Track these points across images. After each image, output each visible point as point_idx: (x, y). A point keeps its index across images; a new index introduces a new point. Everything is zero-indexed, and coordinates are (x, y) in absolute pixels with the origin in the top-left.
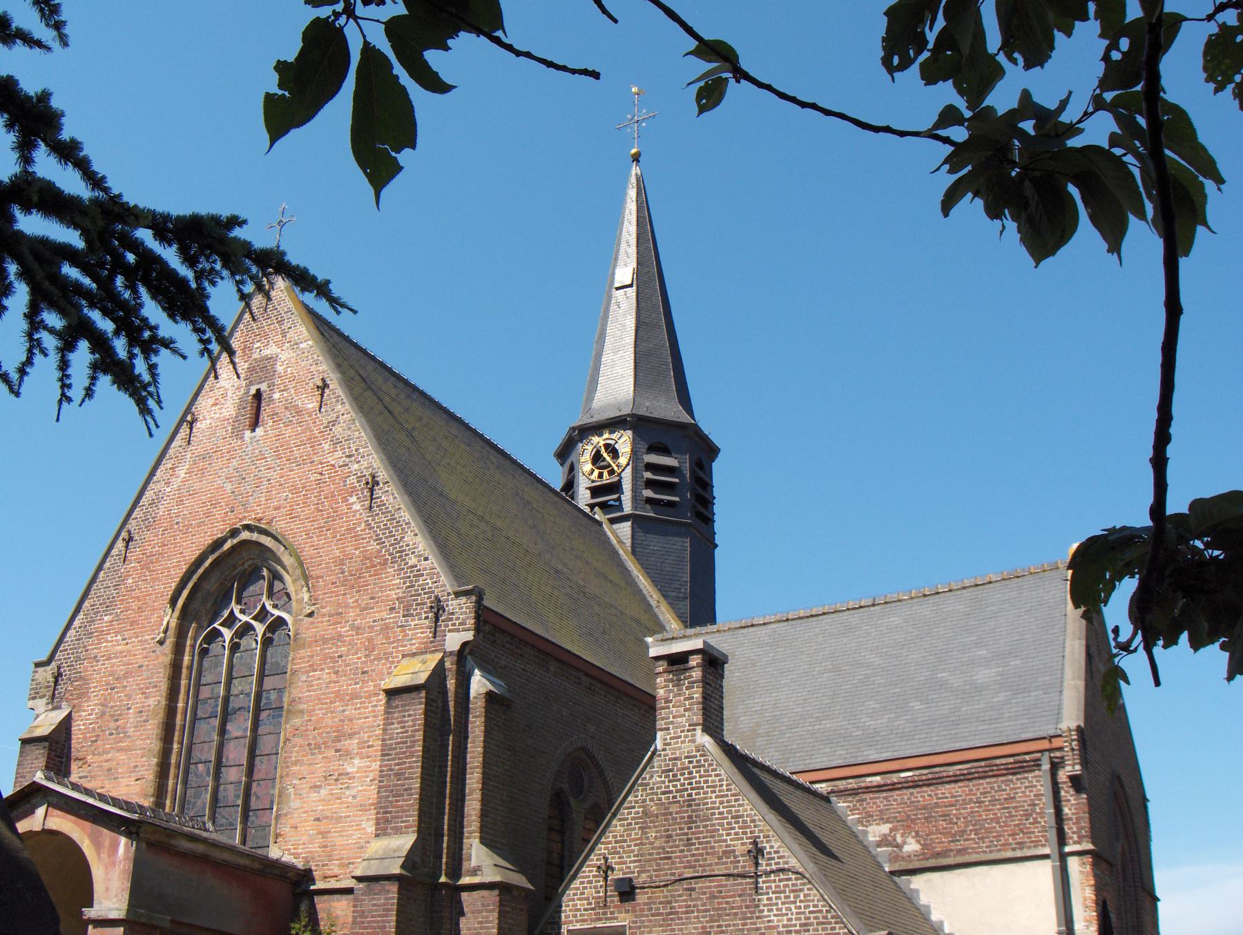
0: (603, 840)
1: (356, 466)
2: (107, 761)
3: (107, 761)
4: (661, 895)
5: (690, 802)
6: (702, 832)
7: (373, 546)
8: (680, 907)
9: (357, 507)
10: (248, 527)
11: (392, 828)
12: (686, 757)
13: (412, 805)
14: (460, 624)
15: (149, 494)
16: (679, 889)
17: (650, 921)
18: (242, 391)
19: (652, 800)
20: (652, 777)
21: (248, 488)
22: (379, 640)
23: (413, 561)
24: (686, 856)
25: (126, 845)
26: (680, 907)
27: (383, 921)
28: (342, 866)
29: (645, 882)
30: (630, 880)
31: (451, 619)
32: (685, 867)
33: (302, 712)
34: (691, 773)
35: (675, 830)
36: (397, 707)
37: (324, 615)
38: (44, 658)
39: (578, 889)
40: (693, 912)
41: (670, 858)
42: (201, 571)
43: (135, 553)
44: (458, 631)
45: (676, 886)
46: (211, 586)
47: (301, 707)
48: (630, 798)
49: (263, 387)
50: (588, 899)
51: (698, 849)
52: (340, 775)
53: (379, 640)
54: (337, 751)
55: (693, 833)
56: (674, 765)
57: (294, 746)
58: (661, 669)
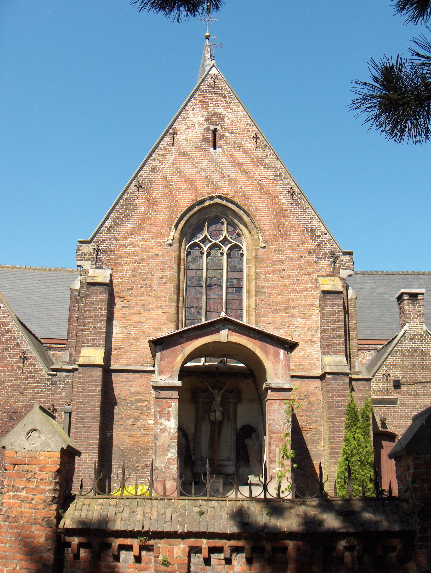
0: (384, 363)
1: (281, 182)
2: (141, 300)
3: (141, 300)
4: (413, 387)
5: (422, 352)
6: (428, 365)
7: (295, 222)
8: (420, 393)
9: (284, 201)
10: (220, 197)
11: (332, 352)
12: (419, 335)
13: (342, 343)
14: (346, 267)
15: (148, 166)
16: (420, 386)
17: (408, 397)
18: (205, 127)
19: (405, 350)
20: (405, 341)
21: (216, 177)
22: (304, 266)
23: (319, 233)
24: (422, 373)
25: (284, 353)
26: (420, 393)
27: (343, 392)
28: (296, 366)
29: (405, 382)
30: (399, 381)
31: (342, 264)
32: (422, 378)
33: (265, 293)
34: (422, 341)
35: (417, 363)
36: (329, 299)
37: (271, 249)
38: (88, 240)
39: (374, 382)
40: (426, 395)
41: (415, 374)
42: (191, 213)
43: (144, 196)
44: (346, 269)
45: (419, 385)
46: (194, 221)
47: (264, 290)
48: (395, 348)
49: (218, 128)
50: (379, 387)
51: (427, 371)
52: (291, 324)
53: (304, 266)
54: (286, 313)
55: (424, 365)
56: (414, 337)
57: (262, 308)
58: (406, 298)
